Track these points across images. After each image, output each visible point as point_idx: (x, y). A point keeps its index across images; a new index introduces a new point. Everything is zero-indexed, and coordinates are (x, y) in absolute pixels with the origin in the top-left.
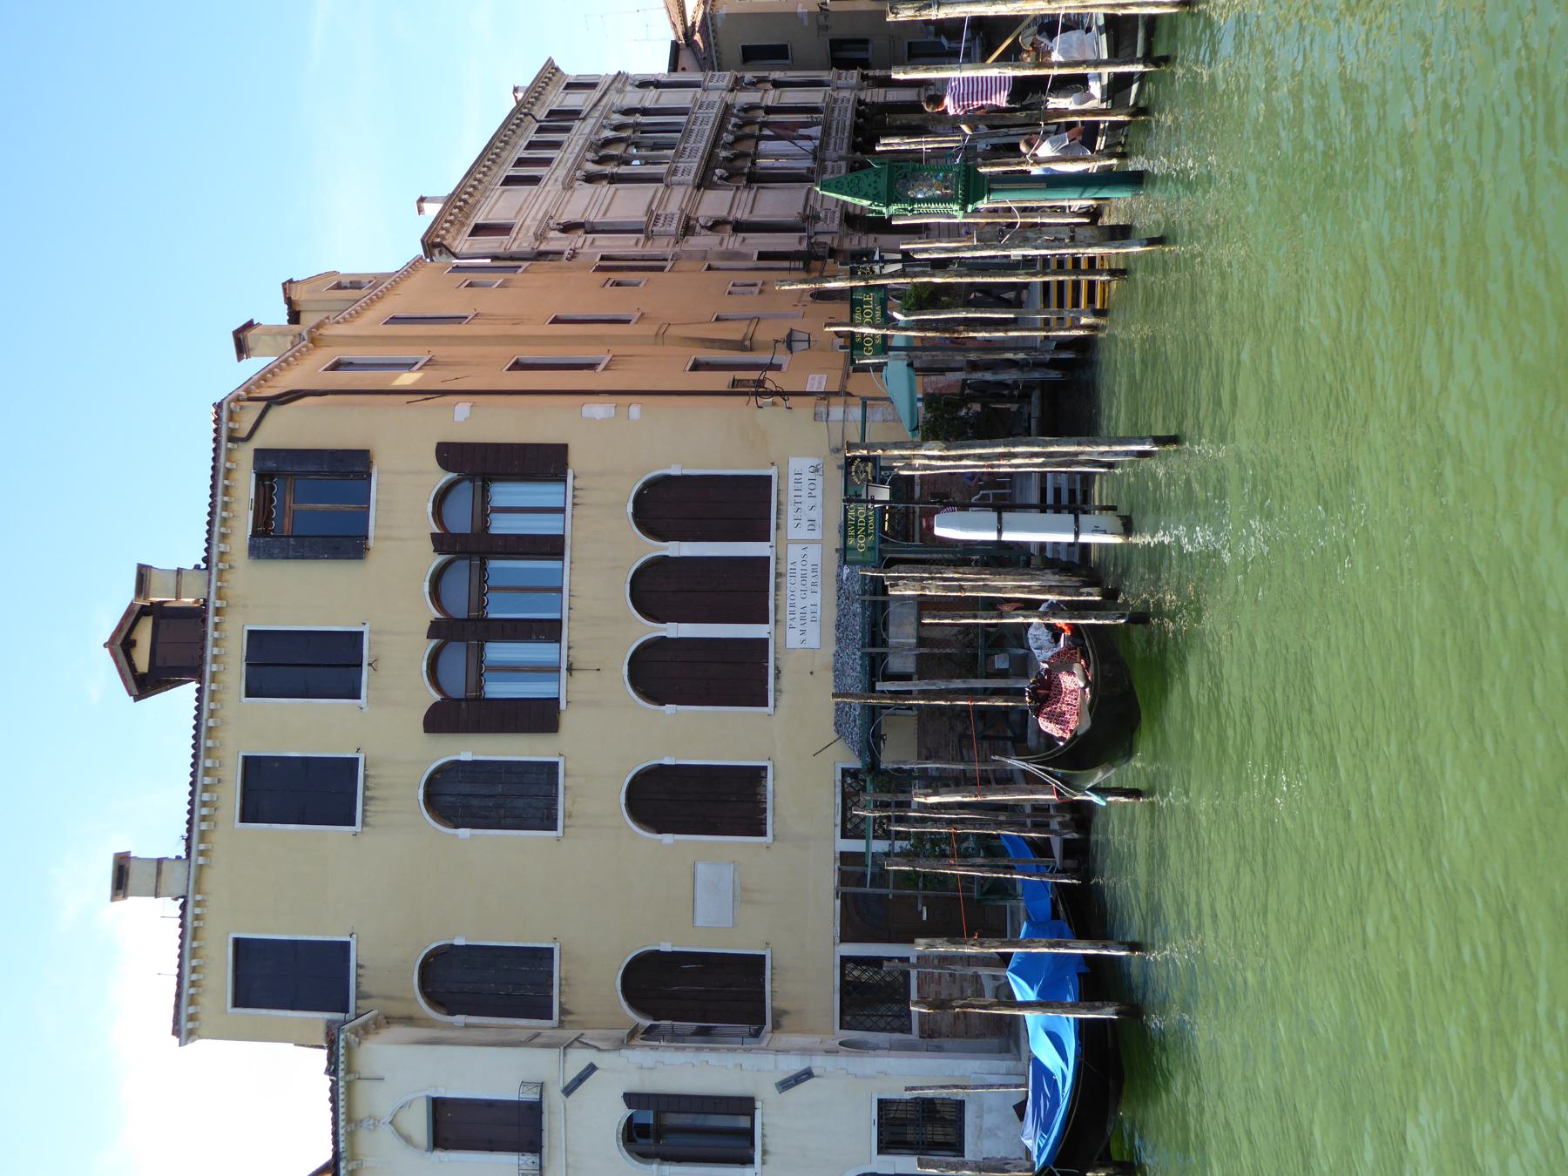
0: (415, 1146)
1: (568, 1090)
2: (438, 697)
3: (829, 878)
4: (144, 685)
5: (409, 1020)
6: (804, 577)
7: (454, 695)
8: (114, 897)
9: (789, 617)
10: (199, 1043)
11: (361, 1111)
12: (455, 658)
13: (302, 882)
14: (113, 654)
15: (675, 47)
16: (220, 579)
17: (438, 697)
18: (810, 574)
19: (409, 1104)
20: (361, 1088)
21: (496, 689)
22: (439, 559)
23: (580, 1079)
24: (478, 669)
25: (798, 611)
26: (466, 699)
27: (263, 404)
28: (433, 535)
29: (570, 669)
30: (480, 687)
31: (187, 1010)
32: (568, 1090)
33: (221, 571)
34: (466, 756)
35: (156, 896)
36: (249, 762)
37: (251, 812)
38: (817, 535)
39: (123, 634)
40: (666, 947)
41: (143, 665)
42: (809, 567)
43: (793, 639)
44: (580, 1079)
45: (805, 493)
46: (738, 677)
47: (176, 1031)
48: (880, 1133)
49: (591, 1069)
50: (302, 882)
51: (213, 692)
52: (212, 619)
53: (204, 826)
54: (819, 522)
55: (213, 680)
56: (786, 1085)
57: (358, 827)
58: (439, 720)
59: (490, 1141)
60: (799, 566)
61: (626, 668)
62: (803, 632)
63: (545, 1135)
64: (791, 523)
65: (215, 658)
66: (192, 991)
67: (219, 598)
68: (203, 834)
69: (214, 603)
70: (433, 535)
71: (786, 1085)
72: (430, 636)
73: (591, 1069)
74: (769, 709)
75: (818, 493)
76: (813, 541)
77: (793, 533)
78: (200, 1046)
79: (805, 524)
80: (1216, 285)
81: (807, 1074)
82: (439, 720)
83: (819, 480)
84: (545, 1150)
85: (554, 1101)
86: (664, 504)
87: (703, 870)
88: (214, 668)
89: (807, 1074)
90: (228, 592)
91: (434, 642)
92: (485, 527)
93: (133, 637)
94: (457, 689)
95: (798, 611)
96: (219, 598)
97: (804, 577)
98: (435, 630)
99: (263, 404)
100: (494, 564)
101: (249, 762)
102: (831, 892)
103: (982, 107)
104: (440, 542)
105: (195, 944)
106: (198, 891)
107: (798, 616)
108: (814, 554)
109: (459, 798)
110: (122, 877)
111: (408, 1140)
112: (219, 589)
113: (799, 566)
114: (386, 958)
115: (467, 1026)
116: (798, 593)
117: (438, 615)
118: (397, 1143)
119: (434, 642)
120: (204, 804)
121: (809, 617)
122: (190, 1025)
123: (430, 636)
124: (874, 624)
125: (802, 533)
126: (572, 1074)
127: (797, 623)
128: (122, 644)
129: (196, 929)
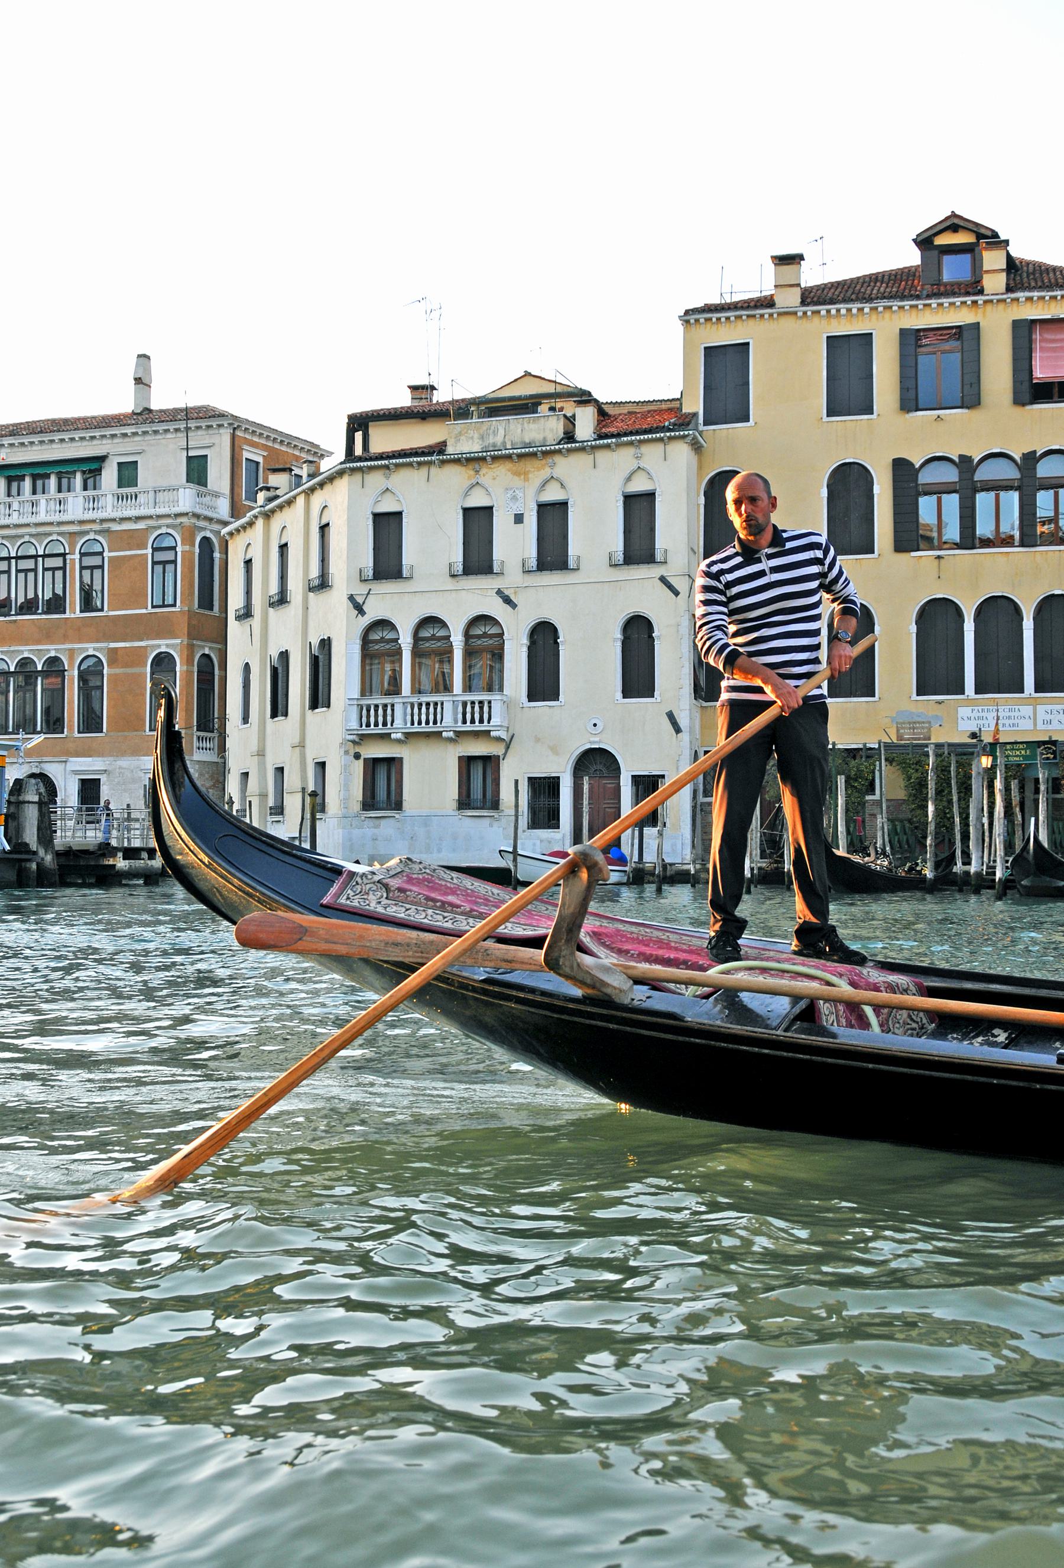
1: (663, 579)
2: (917, 466)
4: (924, 242)
5: (700, 467)
6: (1009, 718)
7: (920, 475)
8: (774, 258)
9: (980, 708)
10: (682, 328)
11: (645, 449)
12: (950, 474)
13: (788, 368)
14: (947, 218)
16: (998, 301)
17: (917, 466)
18: (1011, 722)
19: (651, 478)
20: (660, 447)
22: (1017, 457)
23: (670, 587)
24: (939, 490)
25: (985, 714)
26: (917, 485)
28: (1035, 452)
29: (939, 557)
30: (926, 494)
32: (663, 579)
33: (1004, 300)
34: (876, 489)
38: (1040, 726)
39: (962, 223)
42: (1016, 721)
43: (964, 712)
44: (670, 587)
46: (937, 675)
47: (687, 312)
48: (644, 776)
49: (676, 593)
50: (788, 368)
52: (969, 299)
55: (925, 305)
56: (671, 716)
58: (902, 469)
59: (630, 532)
60: (1016, 714)
61: (941, 596)
62: (969, 719)
63: (636, 566)
64: (1049, 707)
65: (941, 305)
66: (714, 320)
69: (980, 299)
70: (1035, 452)
71: (671, 716)
72: (960, 456)
73: (676, 593)
74: (914, 697)
76: (1035, 724)
77: (1041, 709)
78: (679, 328)
79: (1048, 717)
81: (678, 730)
82: (902, 469)
84: (626, 567)
85: (655, 571)
88: (934, 306)
89: (678, 730)
90: (989, 307)
91: (957, 460)
93: (960, 230)
94: (925, 478)
95: (985, 714)
96: (985, 302)
97: (1009, 718)
98: (965, 460)
100: (1015, 496)
103: (110, 927)
104: (1031, 459)
105: (744, 317)
106: (779, 314)
107: (981, 714)
108: (1026, 725)
110: (788, 260)
111: (629, 479)
112: (991, 301)
113: (1016, 714)
114: (735, 446)
115: (698, 505)
117: (976, 461)
118: (626, 474)
119: (957, 460)
121: (980, 722)
122: (692, 321)
123: (960, 456)
124: (253, 1113)
126: (673, 581)
127: (976, 714)
128: (954, 223)
129: (754, 316)
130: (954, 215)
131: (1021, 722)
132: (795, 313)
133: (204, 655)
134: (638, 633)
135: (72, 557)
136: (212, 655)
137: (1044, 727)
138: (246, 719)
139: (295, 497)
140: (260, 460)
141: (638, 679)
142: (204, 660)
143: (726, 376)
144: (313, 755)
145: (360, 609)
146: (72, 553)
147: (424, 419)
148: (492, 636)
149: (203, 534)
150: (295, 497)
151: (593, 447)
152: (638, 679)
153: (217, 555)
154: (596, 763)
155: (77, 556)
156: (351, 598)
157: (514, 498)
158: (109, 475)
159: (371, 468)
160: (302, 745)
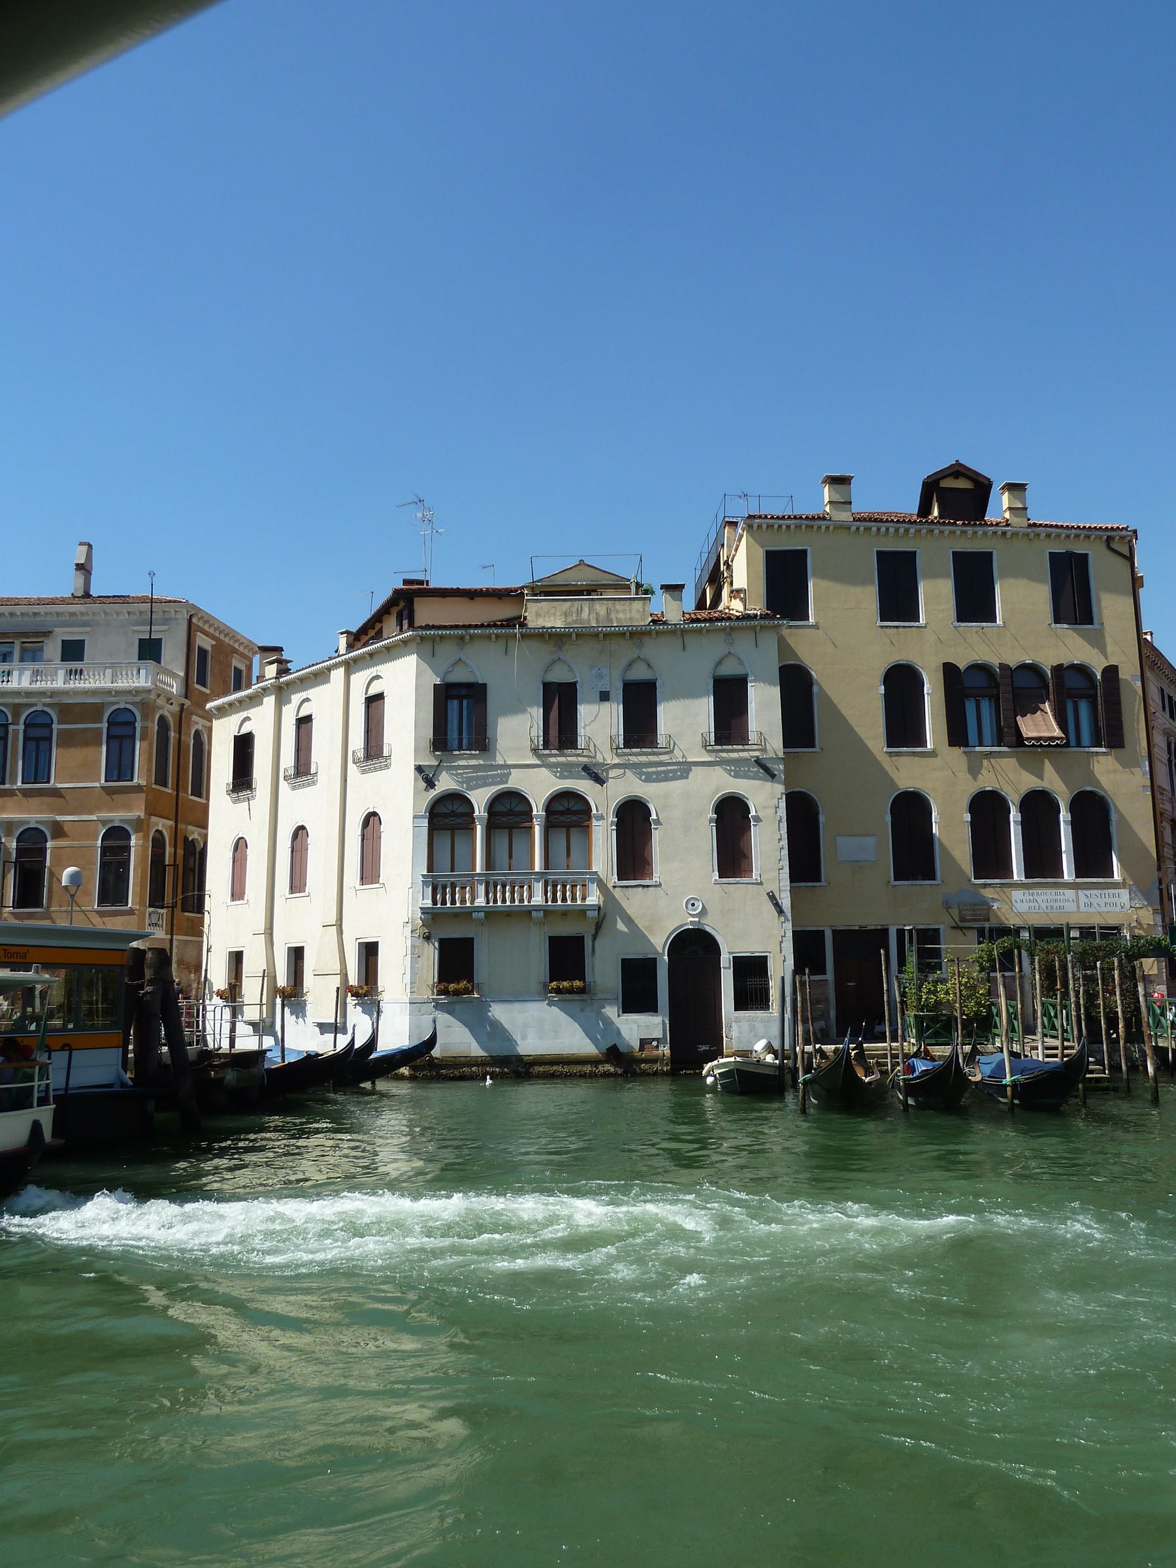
0: (547, 670)
3: (872, 922)
6: (1056, 901)
15: (397, 592)
18: (1058, 904)
19: (741, 663)
21: (970, 707)
24: (977, 696)
27: (1127, 553)
31: (1064, 533)
34: (927, 689)
35: (850, 503)
36: (912, 556)
37: (884, 558)
38: (1082, 908)
40: (822, 819)
41: (944, 484)
45: (1108, 900)
46: (990, 858)
47: (750, 517)
51: (954, 532)
53: (874, 529)
54: (1091, 910)
56: (772, 897)
57: (879, 623)
58: (949, 670)
60: (1062, 897)
67: (768, 526)
68: (868, 529)
75: (1108, 909)
76: (1078, 907)
80: (851, 1236)
81: (780, 911)
83: (1118, 909)
86: (1093, 812)
87: (871, 841)
89: (780, 911)
92: (969, 696)
99: (1127, 553)
101: (912, 556)
102: (863, 924)
108: (1070, 907)
109: (901, 685)
111: (719, 663)
113: (1062, 897)
116: (1045, 897)
120: (907, 530)
121: (1032, 904)
122: (755, 526)
125: (1083, 900)
128: (958, 470)
130: (958, 464)
131: (1066, 905)
132: (849, 528)
133: (157, 831)
134: (732, 817)
135: (16, 727)
136: (165, 832)
137: (1085, 910)
138: (237, 893)
139: (329, 669)
140: (208, 648)
141: (732, 858)
142: (158, 835)
143: (786, 582)
144: (356, 933)
145: (430, 784)
146: (16, 723)
147: (472, 599)
148: (575, 813)
149: (161, 712)
150: (329, 669)
151: (683, 631)
152: (732, 858)
153: (172, 734)
154: (694, 947)
155: (21, 727)
156: (419, 769)
157: (600, 676)
158: (53, 649)
159: (442, 637)
160: (339, 924)
